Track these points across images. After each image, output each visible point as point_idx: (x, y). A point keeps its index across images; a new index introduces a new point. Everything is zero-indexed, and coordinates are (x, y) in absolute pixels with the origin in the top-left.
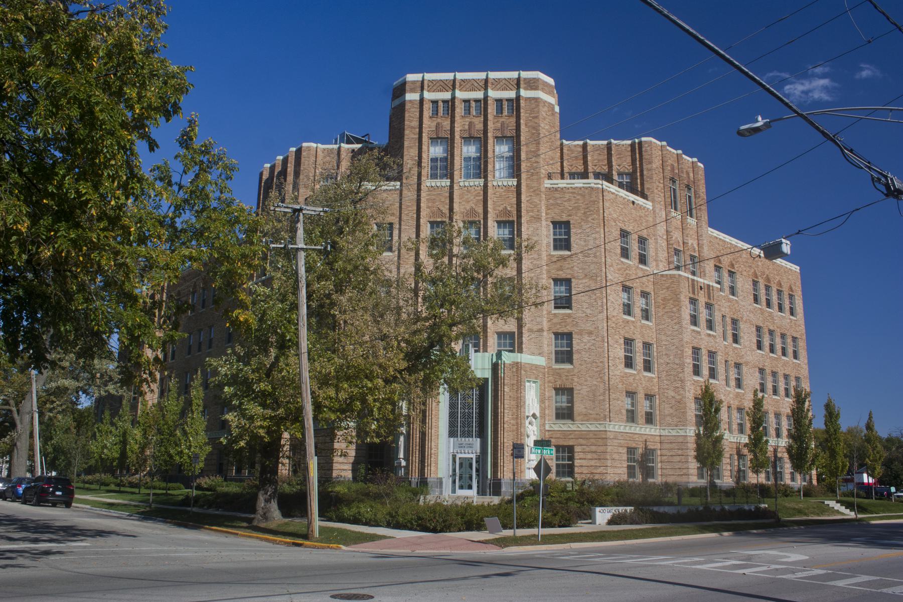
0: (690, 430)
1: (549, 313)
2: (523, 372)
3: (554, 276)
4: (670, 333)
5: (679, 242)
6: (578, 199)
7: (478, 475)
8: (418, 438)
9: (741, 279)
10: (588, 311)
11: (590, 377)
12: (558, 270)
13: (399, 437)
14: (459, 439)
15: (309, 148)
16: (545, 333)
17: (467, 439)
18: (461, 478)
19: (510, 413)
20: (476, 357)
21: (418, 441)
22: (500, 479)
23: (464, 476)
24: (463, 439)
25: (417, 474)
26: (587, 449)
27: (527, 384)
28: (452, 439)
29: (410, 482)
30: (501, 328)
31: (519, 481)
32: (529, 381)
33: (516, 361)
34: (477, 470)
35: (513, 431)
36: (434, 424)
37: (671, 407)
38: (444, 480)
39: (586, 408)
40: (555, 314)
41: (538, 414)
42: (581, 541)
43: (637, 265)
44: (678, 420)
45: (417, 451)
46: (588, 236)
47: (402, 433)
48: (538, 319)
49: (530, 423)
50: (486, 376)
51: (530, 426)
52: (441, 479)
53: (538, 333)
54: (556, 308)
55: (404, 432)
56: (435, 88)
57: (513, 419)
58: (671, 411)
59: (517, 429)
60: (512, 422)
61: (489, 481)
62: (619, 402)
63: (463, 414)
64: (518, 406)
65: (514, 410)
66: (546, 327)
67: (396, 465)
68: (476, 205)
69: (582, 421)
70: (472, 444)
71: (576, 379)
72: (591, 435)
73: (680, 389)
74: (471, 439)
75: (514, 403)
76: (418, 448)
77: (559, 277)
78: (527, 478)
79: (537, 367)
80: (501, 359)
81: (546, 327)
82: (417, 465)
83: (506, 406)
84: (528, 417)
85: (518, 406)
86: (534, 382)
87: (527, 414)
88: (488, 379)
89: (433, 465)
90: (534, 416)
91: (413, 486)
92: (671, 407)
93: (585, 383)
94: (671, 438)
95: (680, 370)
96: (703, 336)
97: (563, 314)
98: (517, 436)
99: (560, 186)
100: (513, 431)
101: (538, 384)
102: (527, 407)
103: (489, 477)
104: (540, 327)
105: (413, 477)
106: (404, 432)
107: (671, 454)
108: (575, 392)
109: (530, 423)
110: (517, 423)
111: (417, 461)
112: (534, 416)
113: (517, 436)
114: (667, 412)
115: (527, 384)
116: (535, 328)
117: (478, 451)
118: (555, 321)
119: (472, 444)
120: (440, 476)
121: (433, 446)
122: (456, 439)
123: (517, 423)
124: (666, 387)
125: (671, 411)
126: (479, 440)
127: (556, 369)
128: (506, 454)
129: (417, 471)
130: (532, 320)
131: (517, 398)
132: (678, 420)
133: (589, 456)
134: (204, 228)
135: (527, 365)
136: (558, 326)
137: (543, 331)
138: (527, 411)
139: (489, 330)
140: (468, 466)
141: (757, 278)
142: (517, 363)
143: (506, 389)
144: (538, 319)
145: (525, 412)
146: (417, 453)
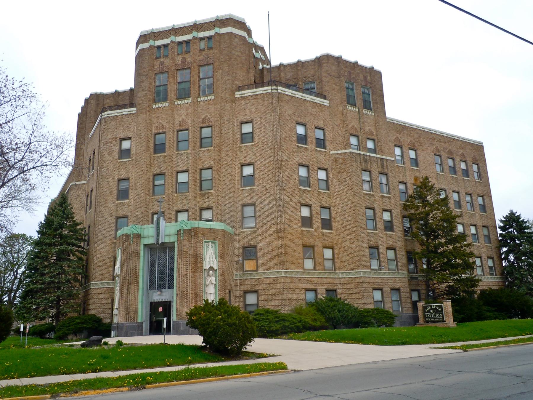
0: (236, 275)
4: (345, 197)
5: (356, 129)
6: (259, 103)
9: (422, 154)
10: (267, 186)
11: (269, 235)
12: (245, 157)
26: (269, 292)
35: (192, 281)
37: (348, 255)
39: (267, 260)
42: (486, 343)
43: (313, 148)
44: (354, 265)
46: (267, 129)
56: (159, 37)
57: (192, 272)
58: (348, 258)
59: (196, 280)
62: (295, 254)
63: (160, 273)
68: (186, 117)
69: (264, 270)
71: (259, 238)
72: (271, 281)
73: (355, 240)
90: (211, 268)
92: (348, 255)
93: (266, 241)
94: (350, 279)
95: (354, 226)
96: (376, 198)
97: (248, 189)
99: (246, 95)
107: (350, 292)
108: (258, 248)
112: (211, 268)
114: (344, 260)
115: (205, 245)
124: (343, 239)
125: (348, 258)
132: (354, 265)
133: (270, 298)
138: (204, 266)
141: (439, 152)
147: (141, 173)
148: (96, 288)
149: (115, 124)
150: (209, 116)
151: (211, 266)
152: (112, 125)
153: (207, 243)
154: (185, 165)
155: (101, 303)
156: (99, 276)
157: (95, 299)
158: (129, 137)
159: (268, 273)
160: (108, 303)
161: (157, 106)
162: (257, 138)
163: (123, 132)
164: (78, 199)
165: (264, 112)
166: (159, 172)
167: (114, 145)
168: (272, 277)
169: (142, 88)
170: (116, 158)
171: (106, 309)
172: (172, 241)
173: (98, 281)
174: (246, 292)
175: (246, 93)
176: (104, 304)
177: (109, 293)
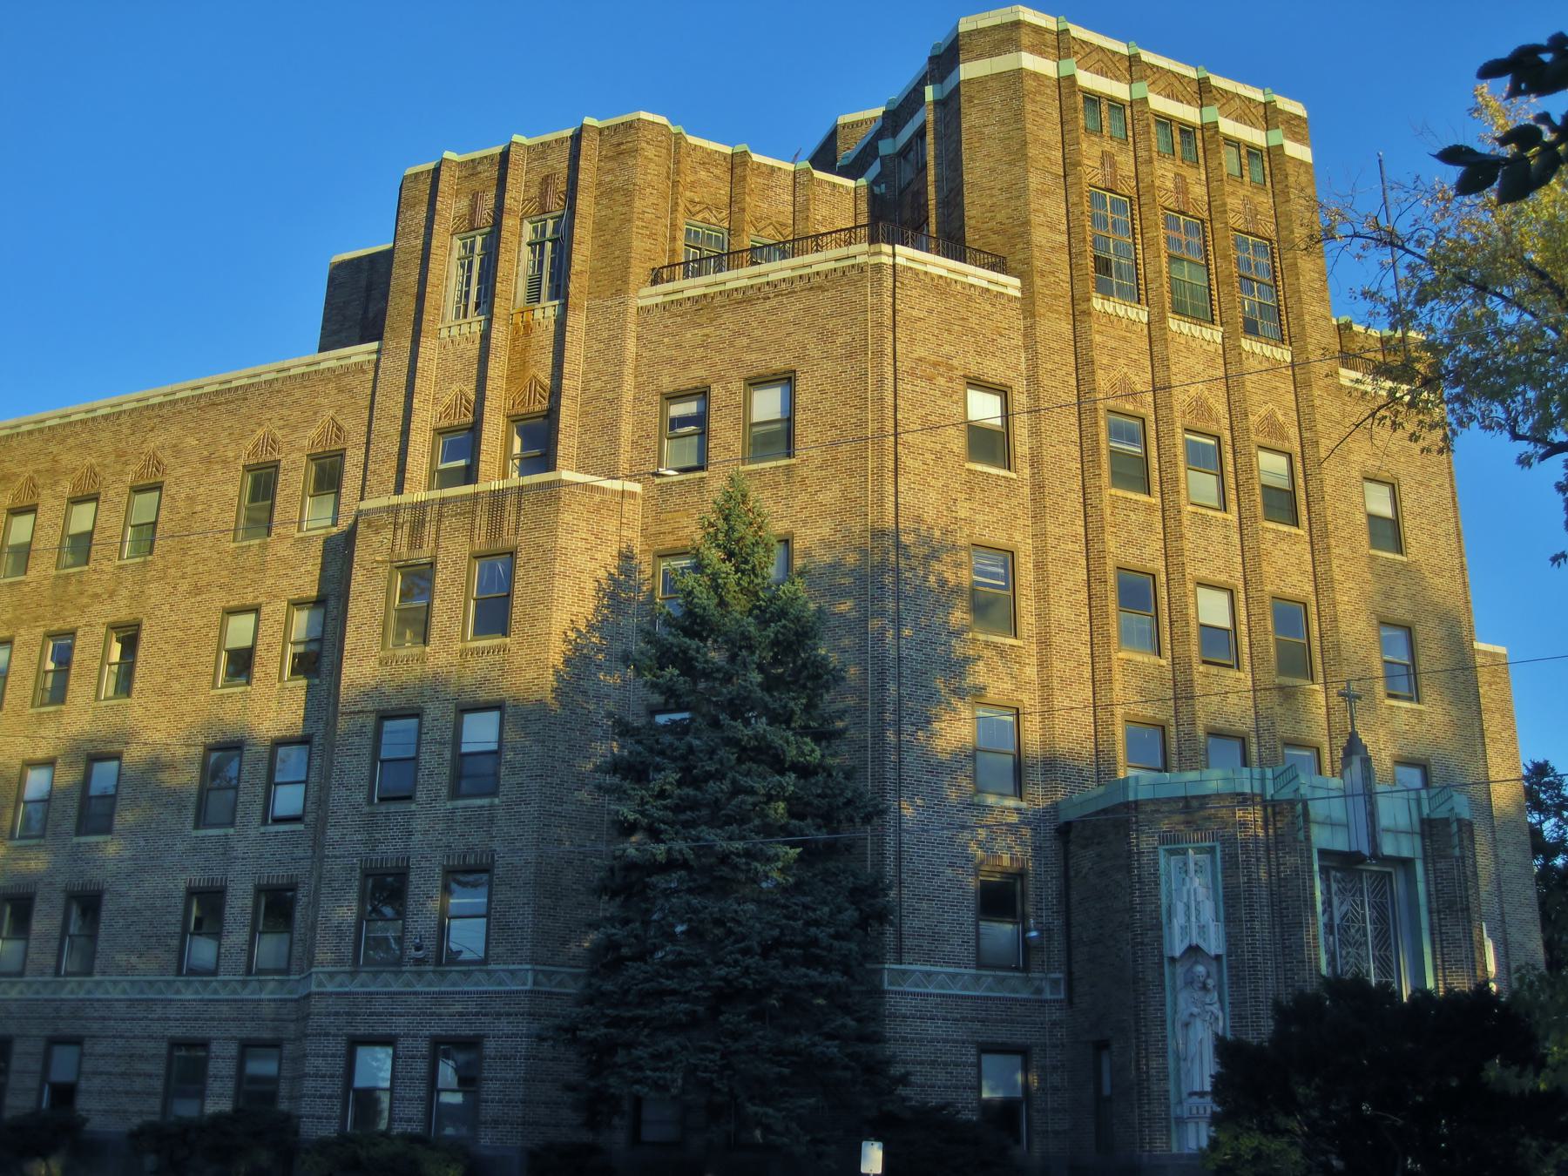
90: (1194, 951)
112: (1194, 951)
147: (1070, 546)
148: (908, 993)
149: (941, 306)
150: (1281, 418)
151: (1194, 942)
152: (930, 311)
153: (1179, 854)
154: (1220, 563)
155: (933, 1063)
156: (916, 942)
157: (905, 1039)
158: (1001, 385)
159: (502, 974)
160: (964, 1064)
161: (1109, 307)
162: (1414, 543)
163: (979, 354)
164: (598, 556)
165: (1422, 466)
166: (1134, 561)
167: (944, 394)
168: (466, 989)
169: (1045, 214)
170: (955, 449)
171: (957, 1087)
172: (1406, 853)
173: (915, 962)
174: (355, 1042)
175: (730, 280)
176: (946, 1064)
177: (964, 1019)
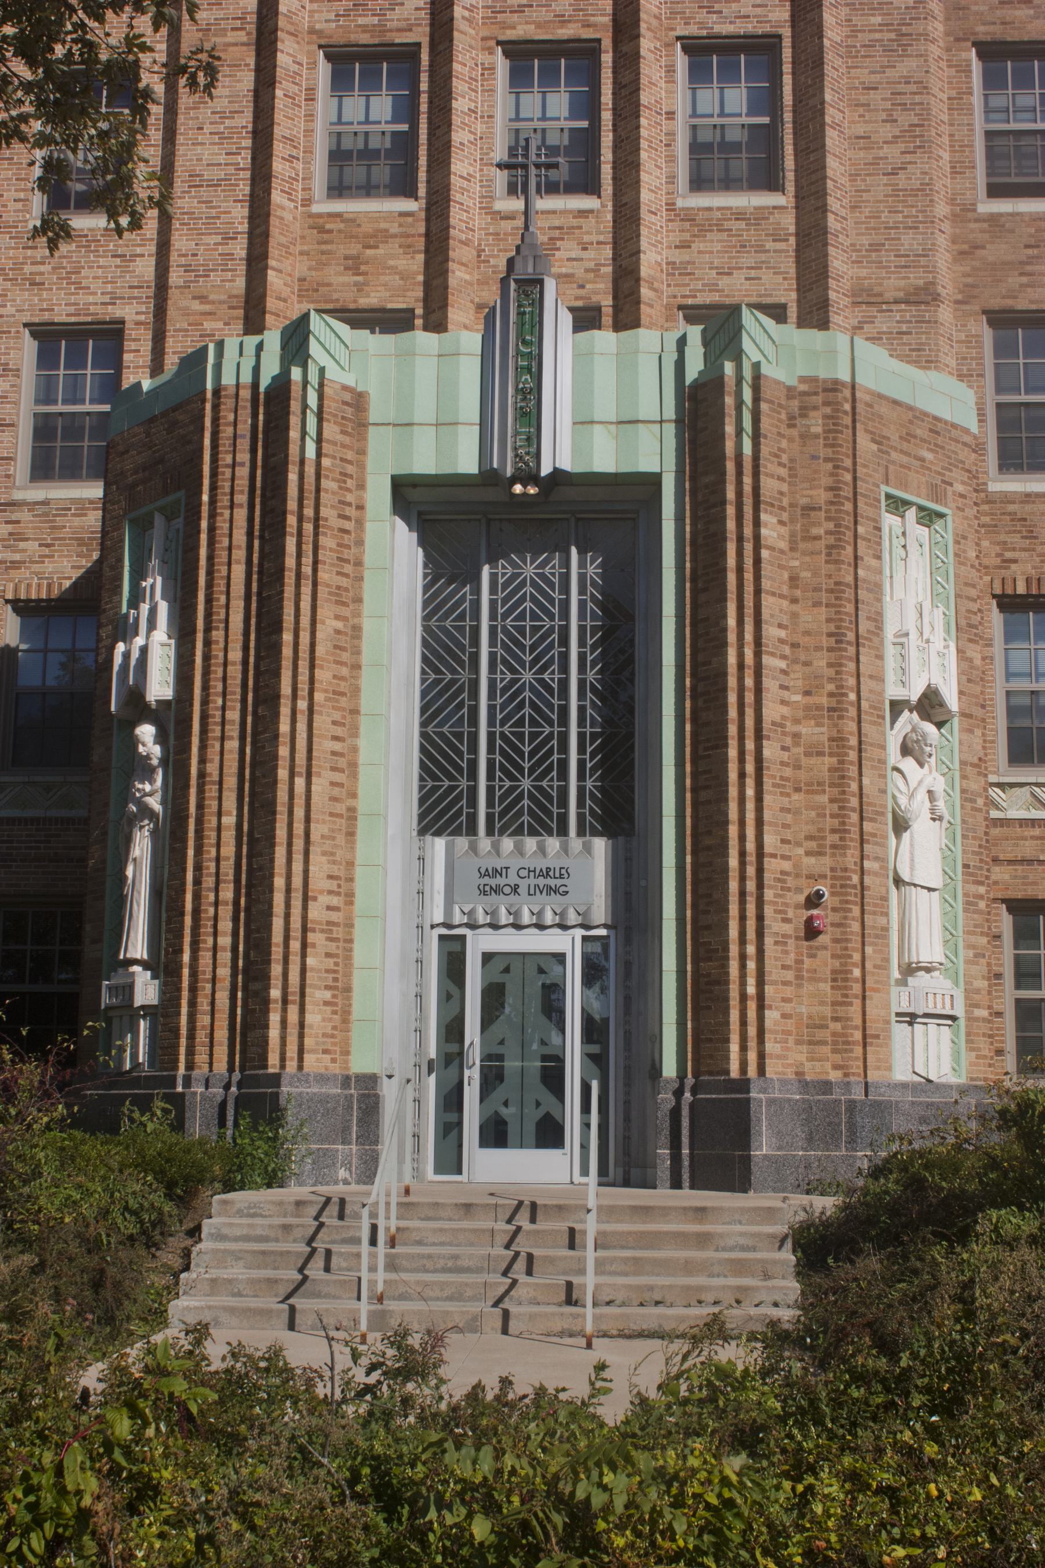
1: (963, 213)
2: (864, 442)
3: (984, 32)
7: (596, 1060)
8: (229, 837)
13: (128, 840)
14: (485, 843)
15: (596, 1318)
16: (945, 314)
17: (531, 843)
18: (492, 1078)
19: (796, 679)
20: (583, 359)
21: (229, 850)
22: (743, 1085)
23: (512, 1065)
24: (508, 844)
25: (221, 1053)
27: (890, 521)
28: (439, 844)
29: (178, 1102)
30: (713, 288)
31: (858, 1094)
32: (898, 506)
33: (823, 374)
34: (593, 1030)
35: (813, 787)
36: (324, 746)
38: (389, 1091)
40: (993, 219)
41: (952, 700)
45: (226, 912)
47: (146, 812)
48: (909, 241)
49: (906, 750)
50: (647, 464)
51: (908, 765)
52: (369, 1081)
53: (911, 312)
54: (995, 191)
55: (155, 803)
57: (811, 712)
60: (810, 731)
61: (666, 1098)
64: (838, 636)
65: (821, 662)
66: (947, 285)
67: (105, 1000)
70: (563, 873)
74: (553, 844)
75: (814, 619)
76: (227, 893)
77: (1012, 35)
78: (901, 1074)
79: (937, 427)
80: (738, 357)
81: (947, 285)
82: (223, 998)
83: (771, 632)
84: (897, 707)
85: (838, 636)
86: (928, 517)
87: (893, 691)
88: (654, 481)
89: (317, 995)
91: (198, 1127)
98: (841, 816)
100: (813, 787)
101: (947, 530)
102: (890, 652)
103: (669, 1068)
104: (917, 278)
105: (201, 1071)
106: (155, 803)
109: (906, 750)
110: (838, 740)
111: (224, 972)
113: (841, 816)
116: (893, 285)
117: (600, 912)
118: (996, 251)
119: (563, 873)
120: (360, 1064)
121: (318, 881)
122: (462, 842)
123: (838, 740)
126: (600, 845)
127: (1007, 498)
128: (774, 925)
129: (222, 1034)
130: (875, 247)
131: (836, 589)
134: (899, 1503)
135: (884, 409)
136: (1014, 280)
137: (936, 298)
139: (645, 292)
140: (535, 1005)
142: (833, 386)
143: (772, 531)
144: (909, 241)
145: (880, 679)
146: (226, 925)
